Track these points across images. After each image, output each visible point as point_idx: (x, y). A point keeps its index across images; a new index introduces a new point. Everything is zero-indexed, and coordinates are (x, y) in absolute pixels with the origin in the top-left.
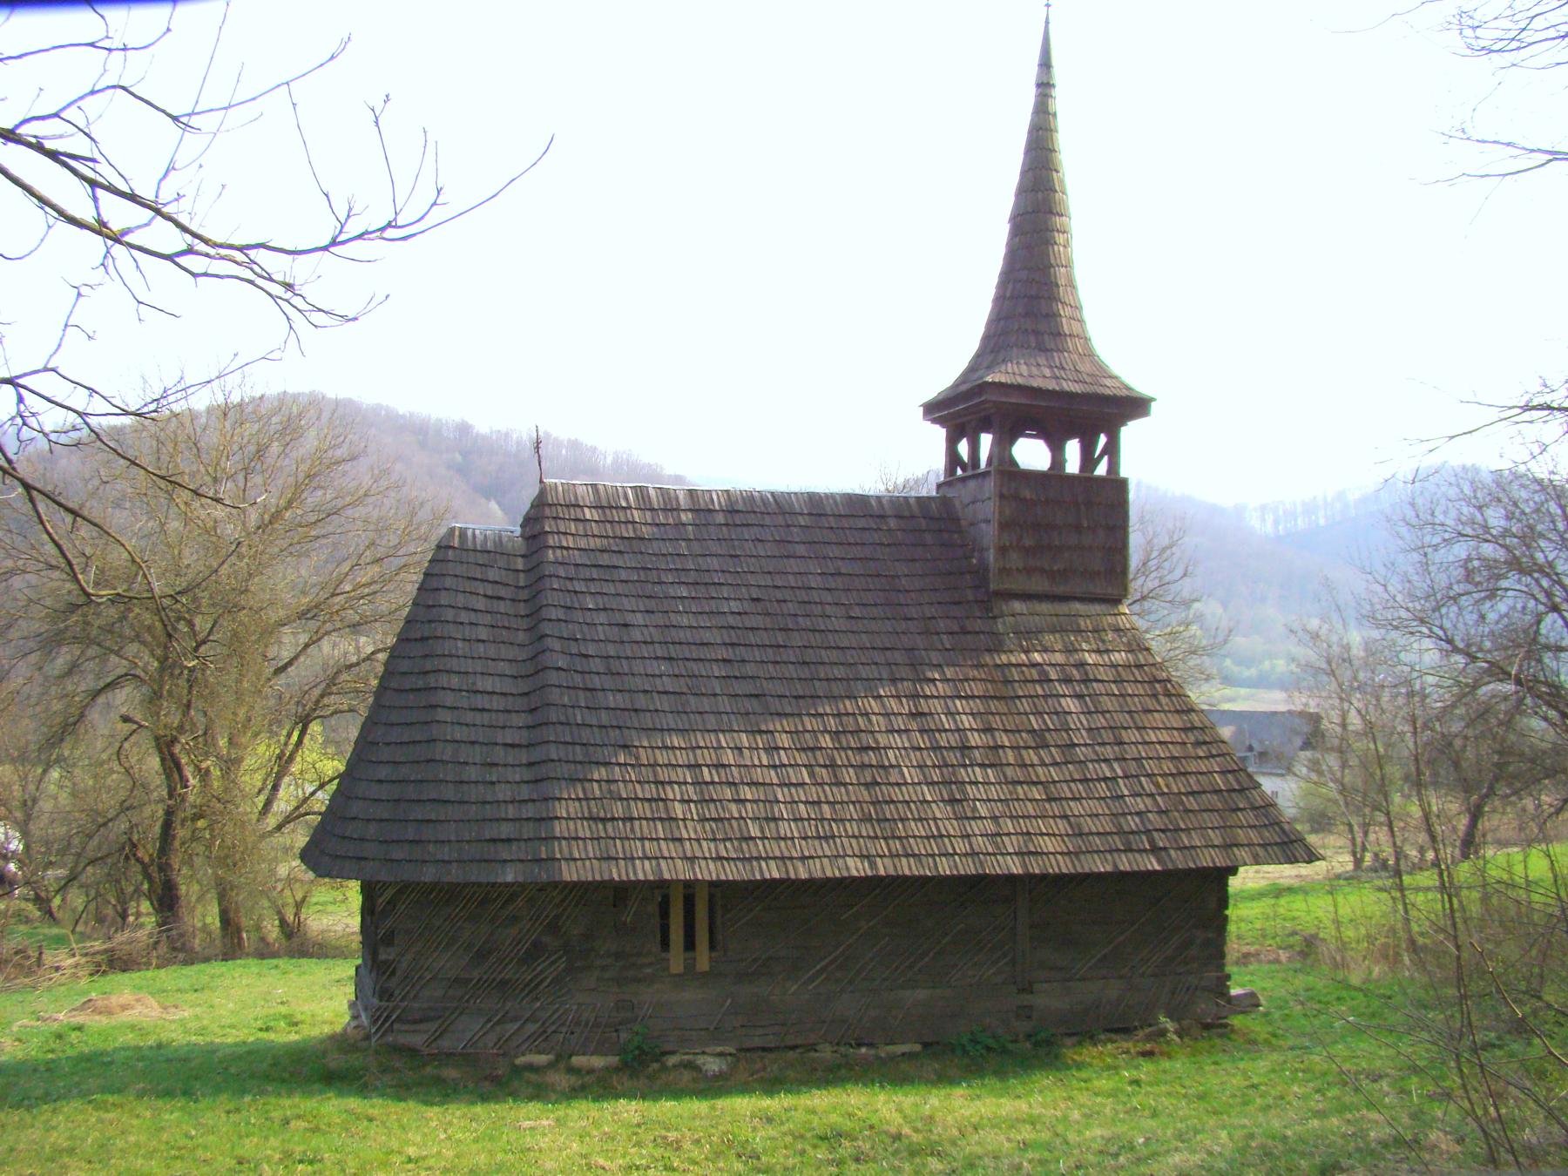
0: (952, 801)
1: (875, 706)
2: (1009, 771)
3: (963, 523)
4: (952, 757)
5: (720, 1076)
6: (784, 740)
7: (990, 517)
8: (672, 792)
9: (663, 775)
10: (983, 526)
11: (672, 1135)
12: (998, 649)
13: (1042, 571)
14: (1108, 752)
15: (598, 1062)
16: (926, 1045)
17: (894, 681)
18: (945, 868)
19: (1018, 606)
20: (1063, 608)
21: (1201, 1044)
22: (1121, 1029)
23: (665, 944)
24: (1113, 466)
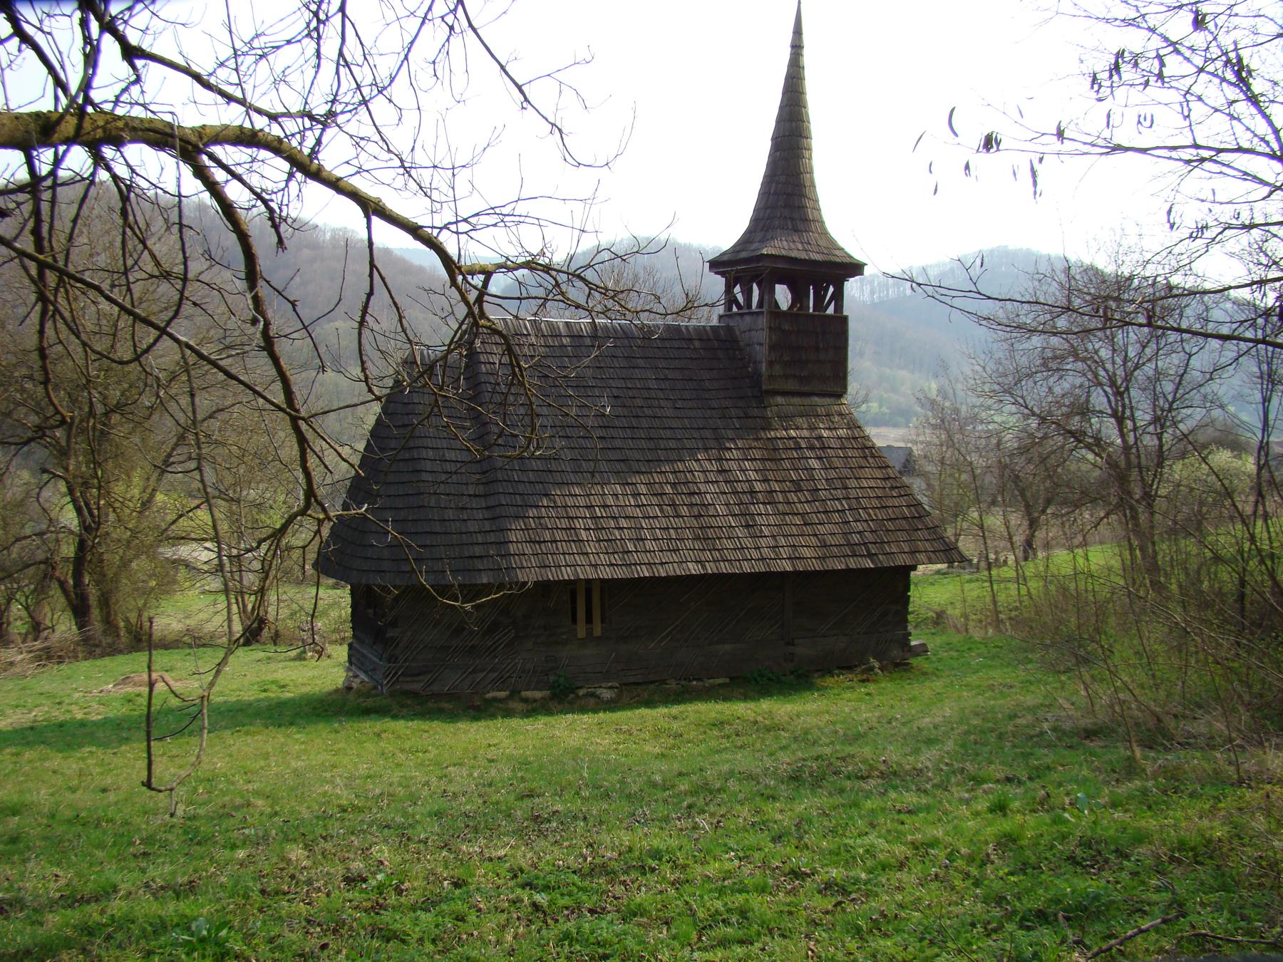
0: (748, 526)
1: (695, 466)
2: (780, 507)
3: (742, 344)
4: (745, 498)
5: (611, 701)
6: (643, 489)
7: (762, 341)
8: (579, 524)
9: (572, 512)
10: (758, 348)
11: (625, 727)
12: (768, 428)
13: (795, 376)
14: (839, 493)
15: (538, 694)
16: (732, 679)
17: (706, 449)
18: (746, 568)
19: (780, 400)
20: (807, 401)
21: (895, 675)
22: (847, 667)
23: (574, 620)
24: (839, 307)
